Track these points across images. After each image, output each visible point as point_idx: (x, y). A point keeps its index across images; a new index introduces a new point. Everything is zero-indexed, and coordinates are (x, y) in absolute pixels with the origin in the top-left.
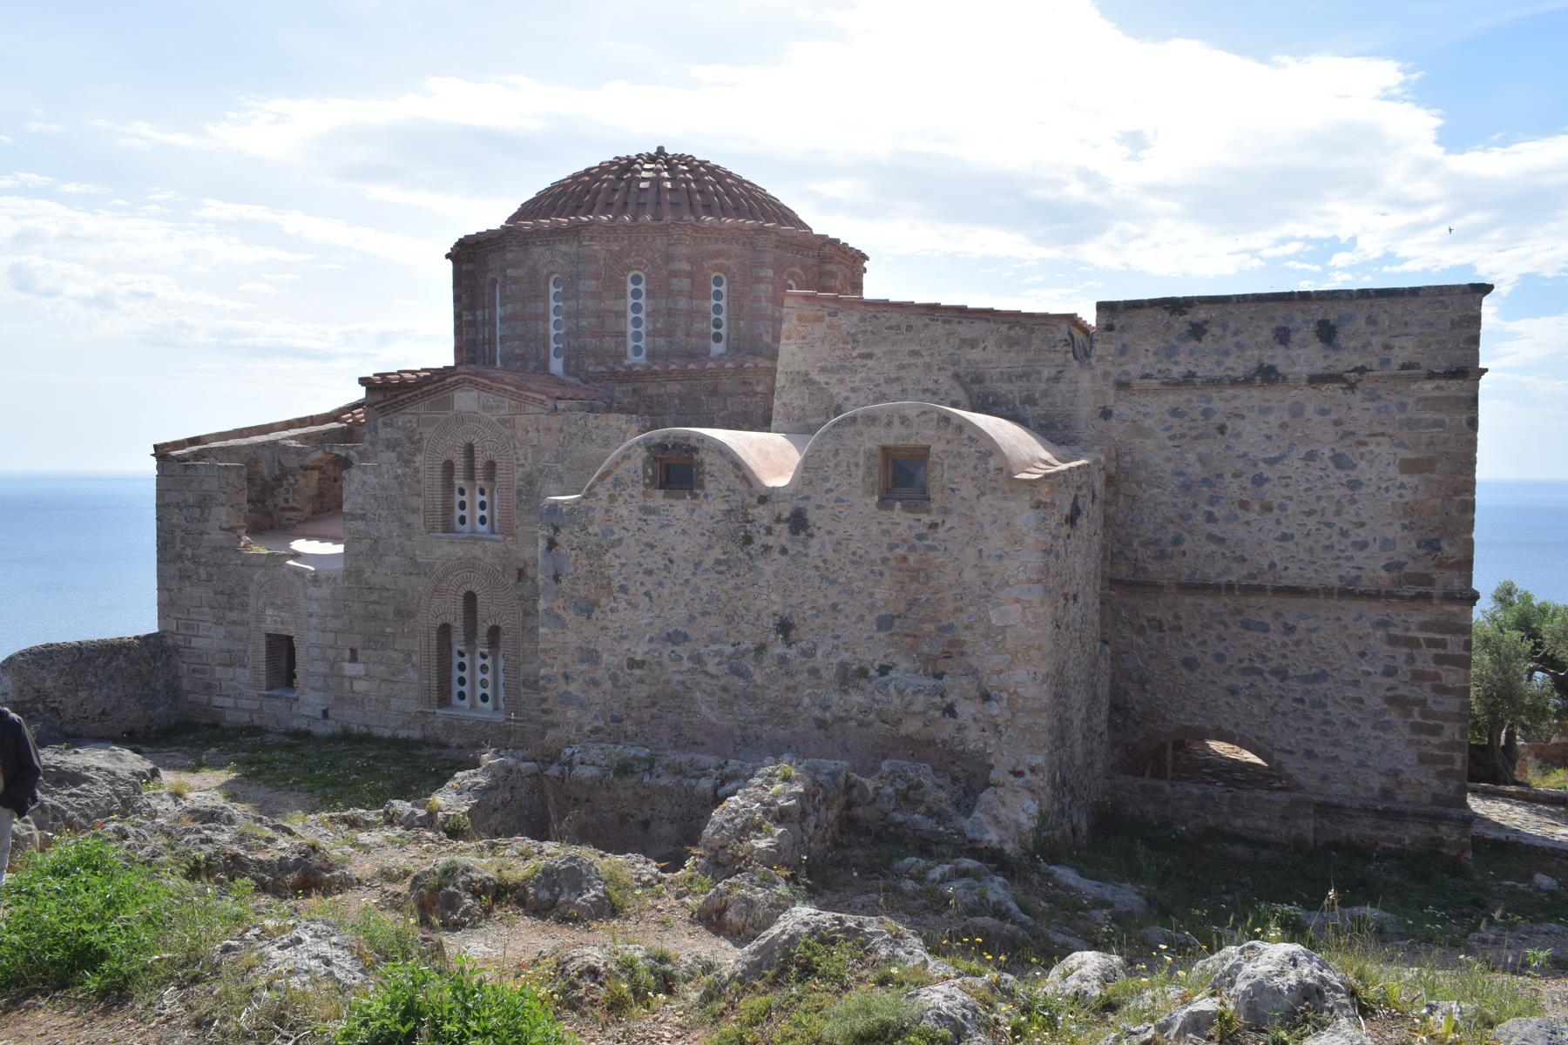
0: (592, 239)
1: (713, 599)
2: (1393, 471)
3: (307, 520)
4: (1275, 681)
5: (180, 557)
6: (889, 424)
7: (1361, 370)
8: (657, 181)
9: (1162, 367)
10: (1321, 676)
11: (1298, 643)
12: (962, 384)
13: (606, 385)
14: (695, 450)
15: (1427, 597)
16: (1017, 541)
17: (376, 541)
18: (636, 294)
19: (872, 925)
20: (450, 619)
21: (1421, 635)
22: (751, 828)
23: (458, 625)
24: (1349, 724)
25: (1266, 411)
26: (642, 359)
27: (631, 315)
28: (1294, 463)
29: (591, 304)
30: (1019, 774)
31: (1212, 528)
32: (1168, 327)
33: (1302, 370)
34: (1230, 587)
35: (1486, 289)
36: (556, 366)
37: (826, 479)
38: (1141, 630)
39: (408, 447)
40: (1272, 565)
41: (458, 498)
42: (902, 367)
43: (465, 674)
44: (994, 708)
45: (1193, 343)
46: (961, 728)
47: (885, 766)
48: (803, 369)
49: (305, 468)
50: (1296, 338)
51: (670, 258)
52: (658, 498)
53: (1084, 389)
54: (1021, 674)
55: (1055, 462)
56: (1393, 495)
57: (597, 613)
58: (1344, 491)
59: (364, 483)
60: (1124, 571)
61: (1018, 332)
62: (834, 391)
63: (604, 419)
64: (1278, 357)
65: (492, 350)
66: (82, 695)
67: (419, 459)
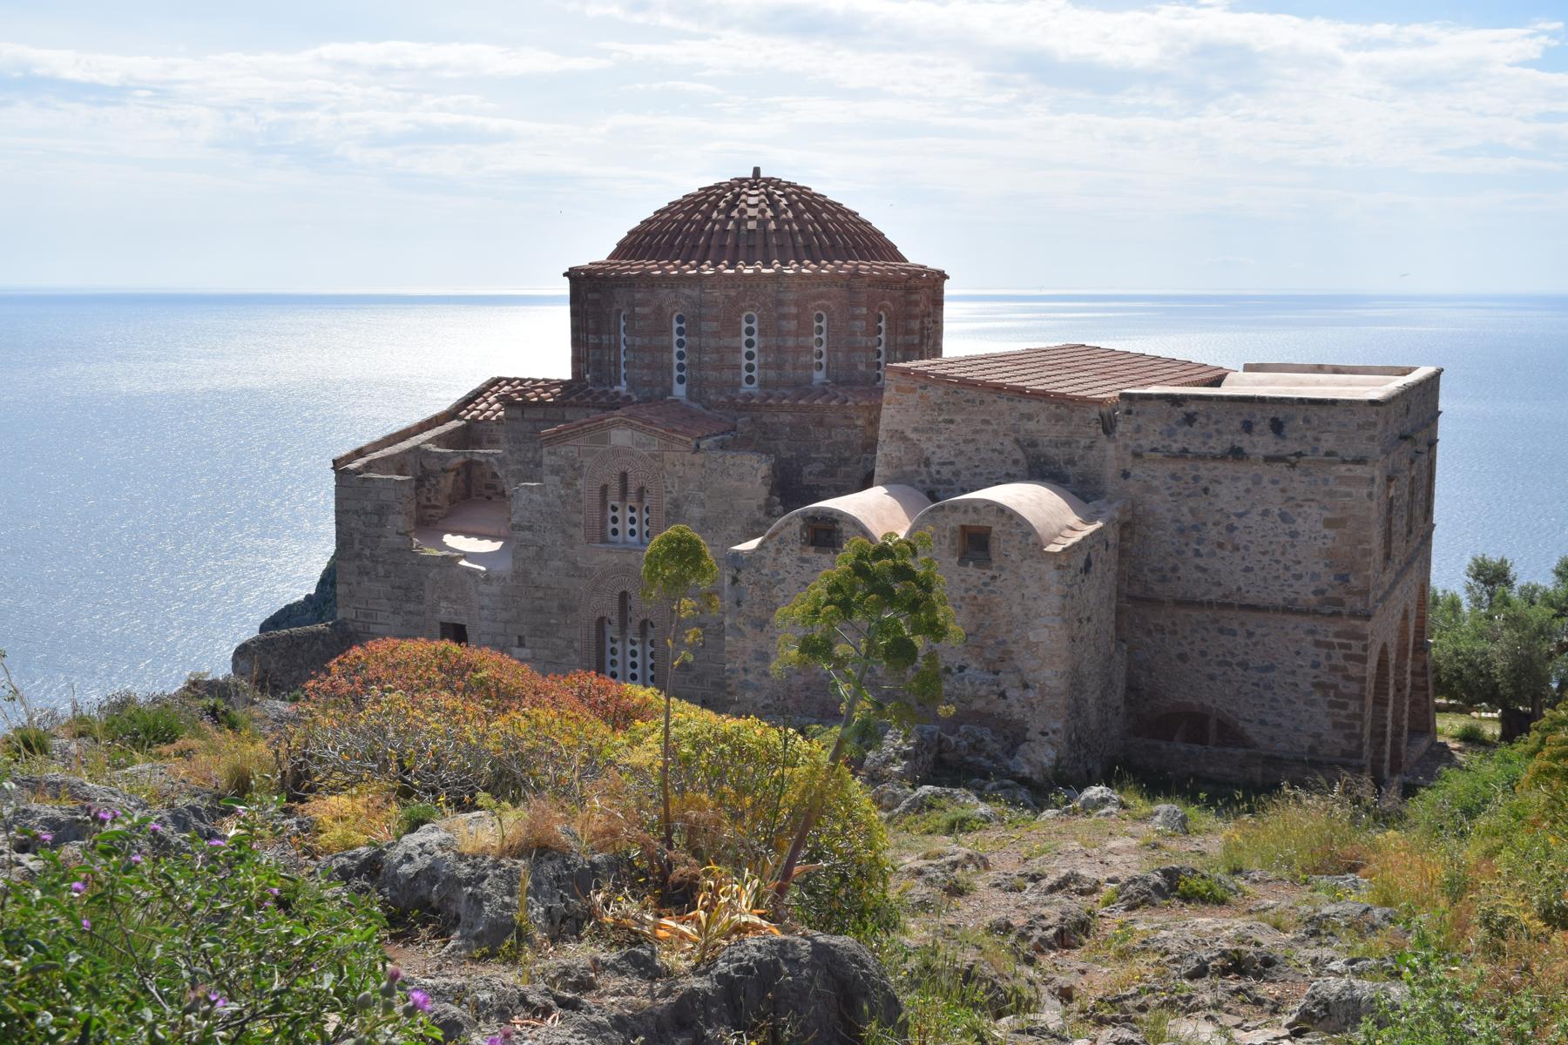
0: (713, 287)
2: (1319, 526)
3: (446, 516)
4: (1240, 671)
5: (359, 556)
6: (966, 512)
7: (1299, 455)
8: (763, 223)
9: (1166, 443)
10: (1271, 668)
11: (1255, 644)
12: (1022, 447)
13: (728, 420)
14: (836, 521)
15: (1339, 614)
16: (1046, 589)
17: (541, 549)
18: (750, 331)
19: (956, 791)
20: (607, 614)
21: (1336, 641)
22: (890, 761)
23: (615, 618)
24: (1289, 701)
25: (1236, 479)
26: (753, 388)
28: (1255, 517)
30: (1044, 734)
31: (1197, 561)
32: (1170, 415)
33: (1260, 451)
34: (1210, 603)
36: (680, 391)
38: (1149, 633)
40: (1239, 589)
41: (611, 514)
42: (976, 432)
43: (630, 659)
44: (1031, 694)
45: (1187, 428)
46: (1009, 706)
47: (962, 729)
48: (900, 428)
49: (445, 471)
50: (1256, 428)
51: (780, 303)
52: (810, 553)
53: (1110, 456)
54: (1047, 672)
55: (1080, 526)
56: (1319, 543)
57: (767, 628)
58: (1288, 539)
59: (531, 501)
60: (1137, 590)
61: (1063, 411)
62: (924, 446)
63: (730, 458)
64: (1244, 441)
65: (618, 371)
67: (580, 483)
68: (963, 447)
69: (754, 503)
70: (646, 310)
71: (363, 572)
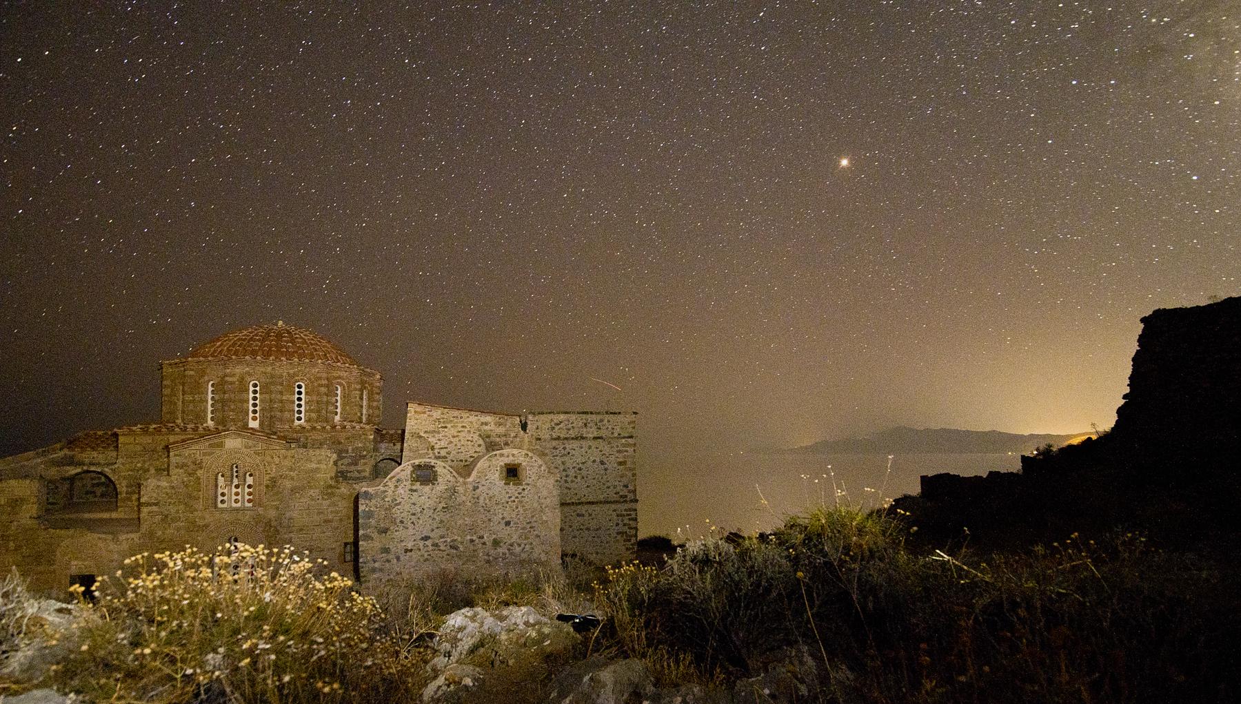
1: (442, 522)
17: (166, 516)
27: (251, 402)
28: (590, 463)
29: (279, 396)
39: (192, 466)
52: (417, 486)
70: (235, 379)
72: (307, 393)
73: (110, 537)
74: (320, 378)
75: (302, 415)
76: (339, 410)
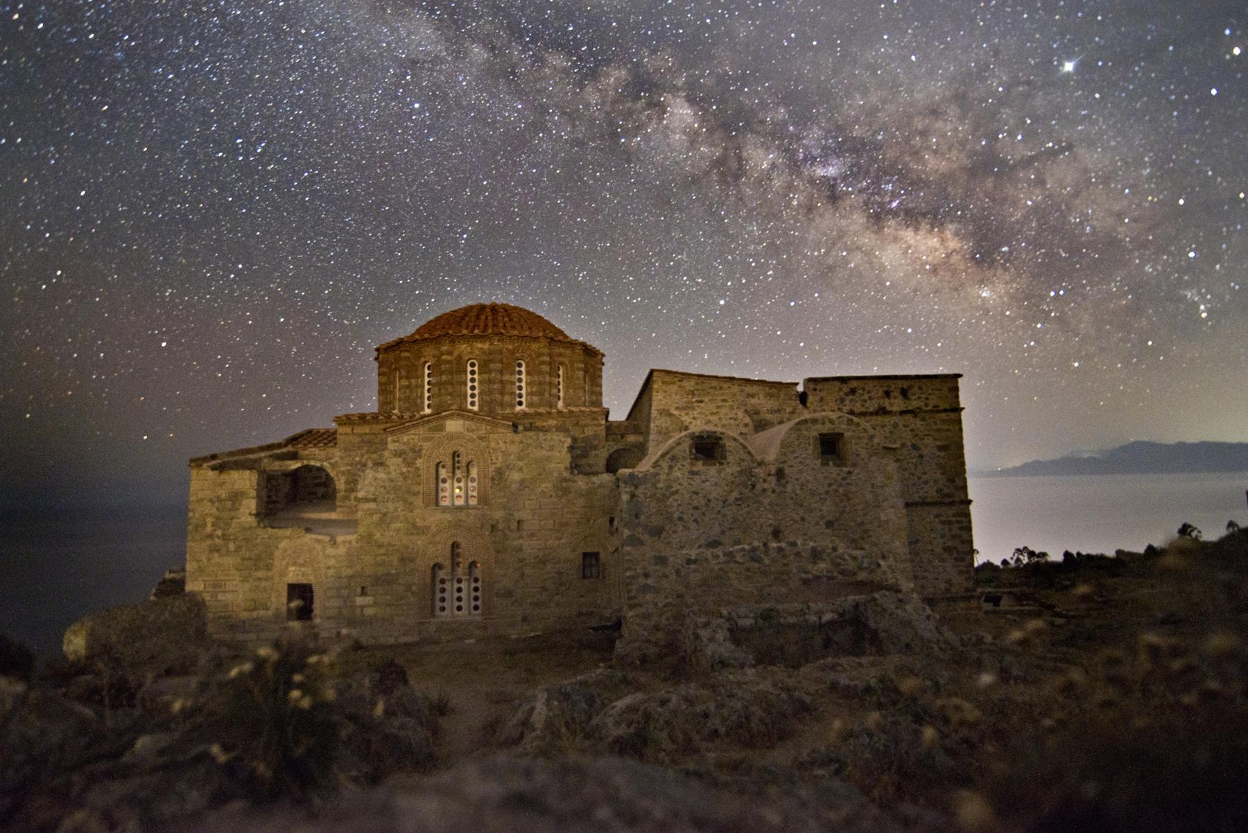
1: (735, 520)
2: (935, 451)
6: (823, 423)
18: (473, 373)
20: (440, 560)
23: (447, 563)
24: (930, 561)
25: (884, 426)
27: (469, 384)
32: (840, 389)
35: (960, 376)
37: (793, 452)
39: (411, 455)
42: (718, 407)
43: (474, 594)
45: (851, 397)
46: (885, 573)
52: (699, 466)
54: (897, 543)
61: (774, 391)
64: (886, 403)
66: (138, 644)
67: (419, 462)
68: (711, 418)
69: (562, 466)
70: (449, 358)
71: (215, 549)
72: (528, 373)
73: (327, 538)
74: (541, 355)
75: (523, 400)
76: (561, 394)
